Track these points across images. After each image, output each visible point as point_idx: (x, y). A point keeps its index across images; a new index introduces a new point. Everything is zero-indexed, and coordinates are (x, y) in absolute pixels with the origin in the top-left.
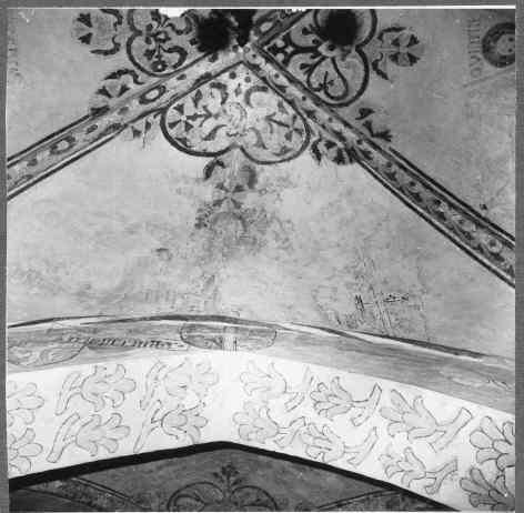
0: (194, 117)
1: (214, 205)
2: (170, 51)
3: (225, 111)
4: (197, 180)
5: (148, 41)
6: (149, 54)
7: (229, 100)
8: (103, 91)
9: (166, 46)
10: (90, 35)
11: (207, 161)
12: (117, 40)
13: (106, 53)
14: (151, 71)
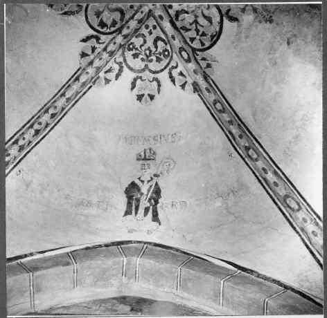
0: (197, 31)
1: (256, 12)
2: (156, 47)
3: (193, 11)
4: (239, 26)
5: (151, 61)
7: (186, 9)
8: (183, 86)
9: (153, 49)
10: (149, 95)
11: (226, 21)
12: (151, 80)
13: (159, 85)
14: (169, 58)
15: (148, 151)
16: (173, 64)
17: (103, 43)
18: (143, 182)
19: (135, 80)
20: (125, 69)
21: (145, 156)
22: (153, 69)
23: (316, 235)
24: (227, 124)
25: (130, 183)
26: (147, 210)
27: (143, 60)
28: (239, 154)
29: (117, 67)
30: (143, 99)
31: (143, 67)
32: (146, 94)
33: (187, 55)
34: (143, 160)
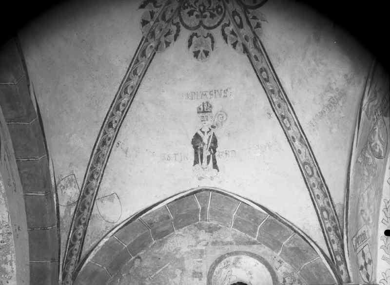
5: (205, 17)
6: (212, 16)
8: (234, 45)
9: (207, 6)
10: (204, 51)
13: (213, 42)
15: (206, 105)
16: (225, 21)
17: (161, 6)
18: (203, 132)
19: (191, 37)
20: (182, 28)
21: (204, 108)
22: (207, 25)
23: (319, 198)
24: (270, 92)
25: (194, 135)
26: (208, 157)
27: (197, 16)
28: (276, 115)
29: (174, 28)
30: (200, 55)
31: (197, 23)
32: (202, 51)
33: (239, 20)
34: (202, 112)
